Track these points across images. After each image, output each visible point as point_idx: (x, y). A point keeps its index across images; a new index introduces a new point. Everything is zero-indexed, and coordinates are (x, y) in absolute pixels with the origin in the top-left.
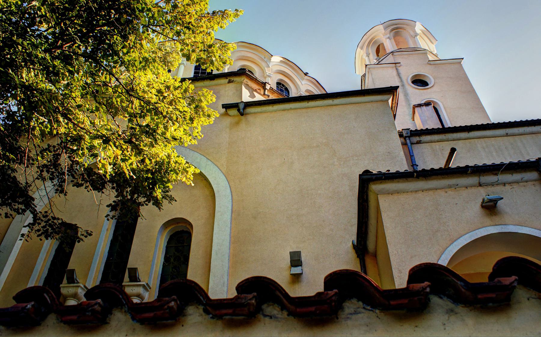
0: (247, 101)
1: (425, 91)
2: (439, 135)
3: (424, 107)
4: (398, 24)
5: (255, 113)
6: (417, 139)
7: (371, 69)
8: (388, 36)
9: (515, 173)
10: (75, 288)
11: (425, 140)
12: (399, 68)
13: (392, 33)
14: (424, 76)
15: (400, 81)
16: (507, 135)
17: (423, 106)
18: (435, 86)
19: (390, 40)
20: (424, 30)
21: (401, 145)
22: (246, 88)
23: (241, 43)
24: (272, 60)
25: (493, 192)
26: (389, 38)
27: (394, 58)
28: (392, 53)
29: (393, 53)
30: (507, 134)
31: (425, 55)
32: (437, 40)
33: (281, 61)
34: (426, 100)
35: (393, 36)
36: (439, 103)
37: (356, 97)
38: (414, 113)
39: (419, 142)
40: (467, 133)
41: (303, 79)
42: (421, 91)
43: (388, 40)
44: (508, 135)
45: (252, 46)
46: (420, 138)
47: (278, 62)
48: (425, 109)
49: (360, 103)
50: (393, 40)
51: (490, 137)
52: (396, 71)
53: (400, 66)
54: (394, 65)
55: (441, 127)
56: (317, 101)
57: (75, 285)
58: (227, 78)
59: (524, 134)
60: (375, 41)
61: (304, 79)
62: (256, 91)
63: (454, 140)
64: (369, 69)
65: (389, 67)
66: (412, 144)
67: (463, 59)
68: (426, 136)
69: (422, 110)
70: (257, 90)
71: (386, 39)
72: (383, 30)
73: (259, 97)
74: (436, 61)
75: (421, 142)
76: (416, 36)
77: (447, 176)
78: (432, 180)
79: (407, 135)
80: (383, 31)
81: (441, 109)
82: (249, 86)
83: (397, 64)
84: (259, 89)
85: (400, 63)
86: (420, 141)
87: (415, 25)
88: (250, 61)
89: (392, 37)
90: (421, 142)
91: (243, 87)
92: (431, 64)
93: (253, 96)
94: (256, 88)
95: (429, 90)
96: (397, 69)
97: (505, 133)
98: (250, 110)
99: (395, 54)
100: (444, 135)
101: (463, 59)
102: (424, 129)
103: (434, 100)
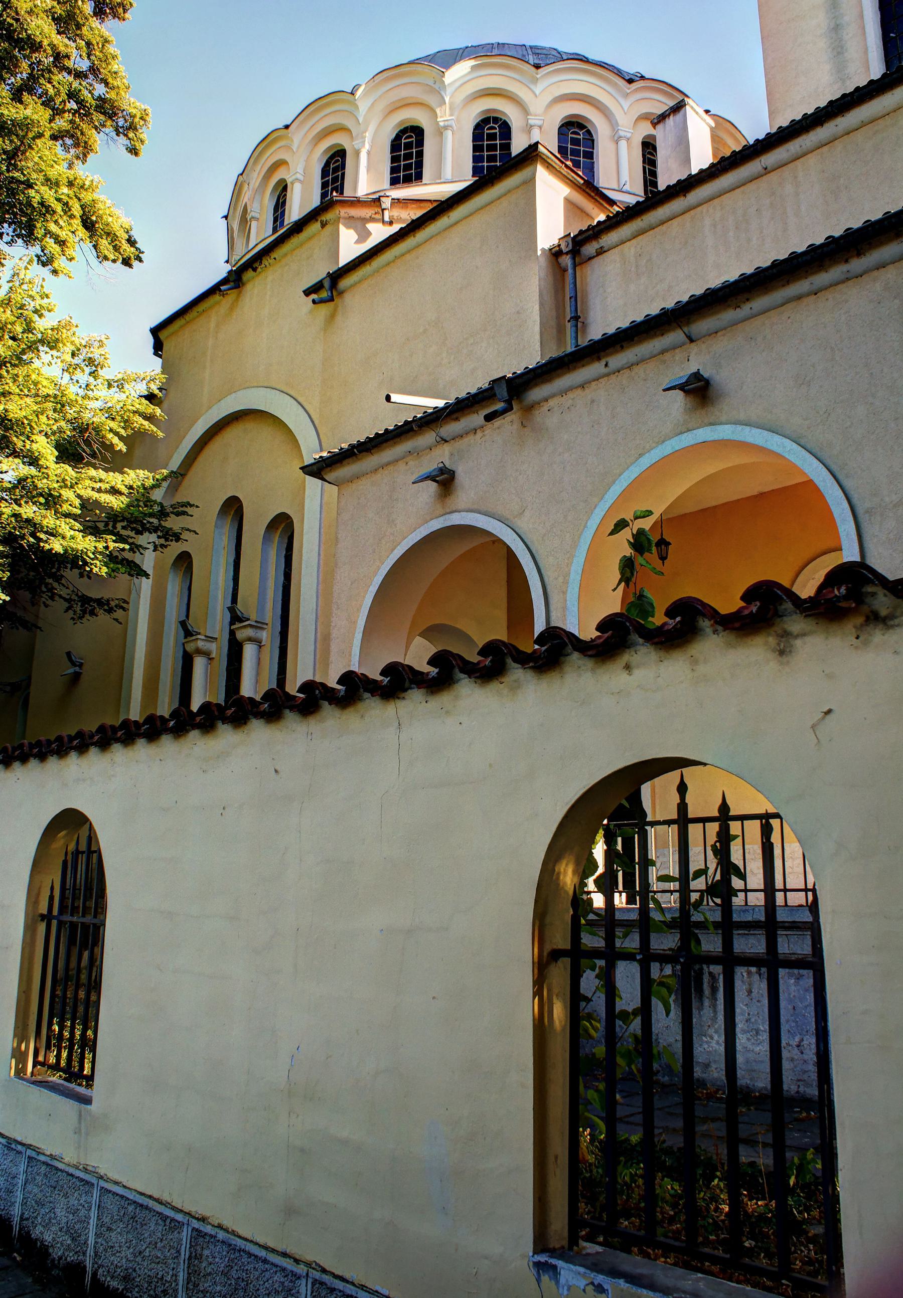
0: (358, 255)
5: (352, 286)
9: (482, 409)
10: (194, 642)
11: (609, 242)
16: (767, 171)
17: (669, 115)
22: (348, 227)
23: (381, 74)
24: (446, 83)
25: (442, 456)
30: (766, 169)
33: (474, 68)
39: (601, 252)
40: (682, 198)
41: (535, 81)
44: (769, 168)
45: (402, 69)
46: (598, 242)
47: (469, 73)
49: (492, 202)
56: (426, 226)
57: (194, 638)
58: (317, 220)
59: (804, 155)
61: (537, 79)
62: (372, 220)
63: (663, 223)
68: (609, 235)
70: (373, 216)
73: (379, 233)
77: (399, 440)
78: (383, 450)
82: (355, 216)
84: (376, 213)
88: (410, 104)
91: (341, 227)
93: (364, 235)
94: (370, 214)
97: (760, 168)
98: (344, 283)
100: (639, 219)
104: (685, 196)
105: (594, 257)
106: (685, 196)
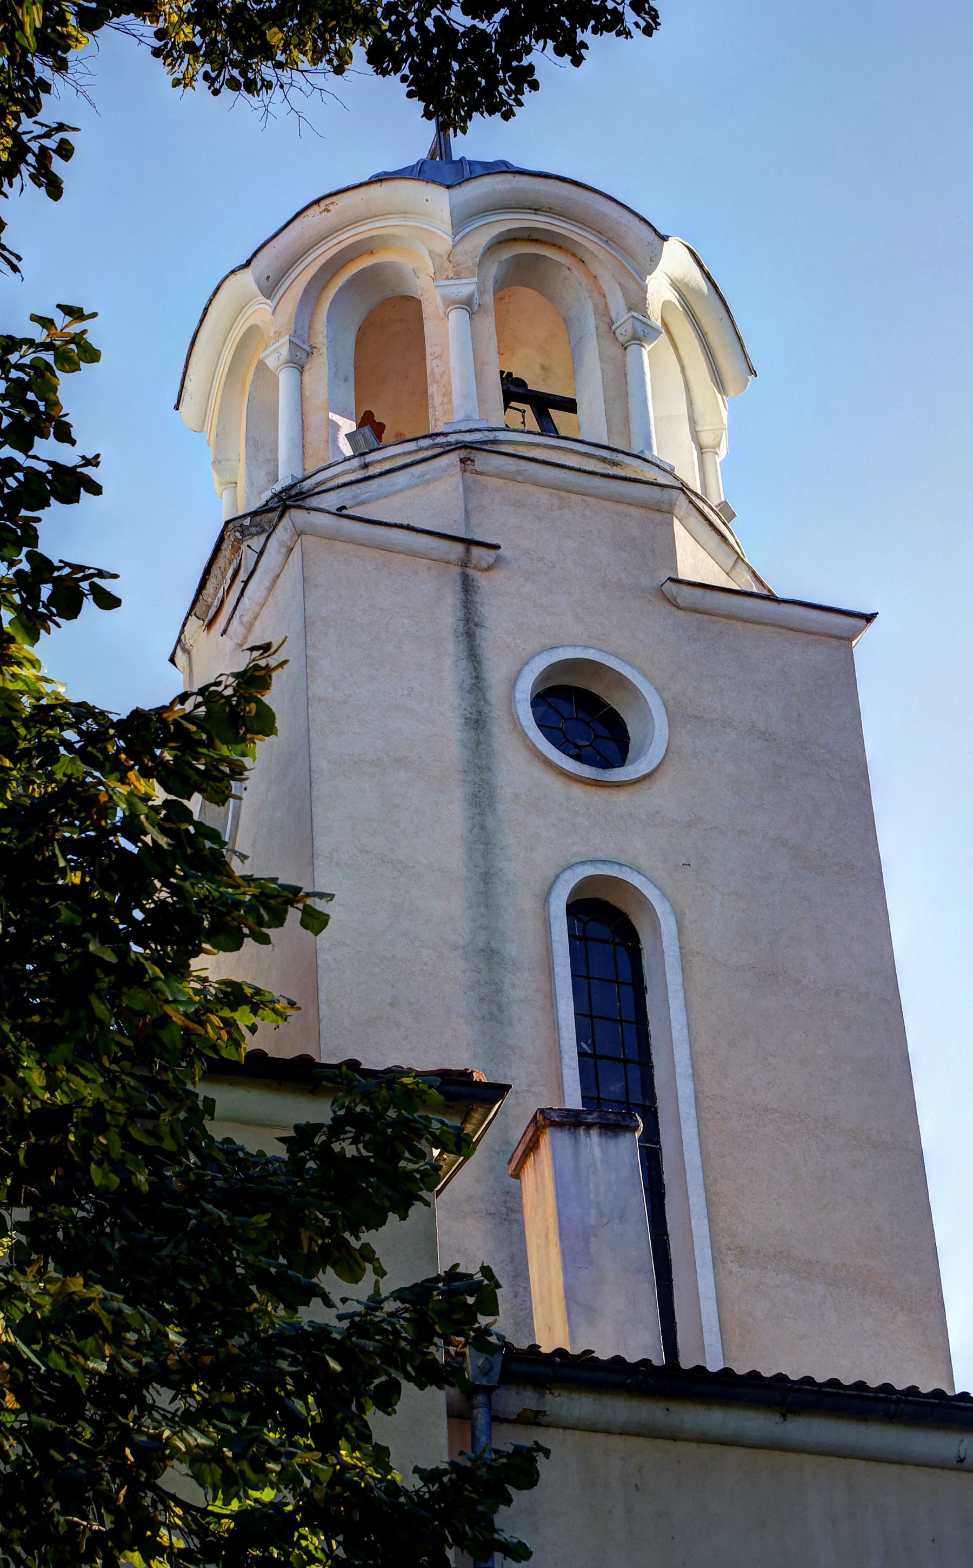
1: (598, 796)
2: (635, 1403)
3: (594, 1133)
4: (550, 211)
6: (527, 1399)
7: (308, 540)
8: (466, 287)
12: (482, 580)
13: (493, 270)
14: (620, 681)
15: (469, 681)
18: (662, 785)
19: (472, 315)
20: (697, 292)
21: (445, 1416)
26: (467, 304)
27: (467, 490)
28: (463, 453)
29: (474, 455)
30: (961, 1460)
31: (658, 516)
32: (753, 372)
34: (590, 871)
35: (496, 282)
36: (661, 908)
37: (269, 1088)
38: (532, 1146)
42: (577, 790)
43: (457, 317)
46: (542, 1396)
48: (597, 1151)
50: (488, 324)
51: (878, 1460)
52: (460, 595)
53: (489, 568)
54: (459, 548)
55: (659, 1360)
60: (374, 268)
63: (704, 1439)
64: (300, 534)
65: (422, 556)
66: (496, 1419)
67: (869, 618)
68: (576, 1396)
69: (576, 1155)
71: (451, 303)
72: (449, 228)
74: (708, 593)
75: (542, 1419)
76: (638, 339)
79: (484, 1381)
80: (444, 238)
81: (660, 953)
83: (476, 551)
85: (496, 547)
86: (538, 1413)
87: (654, 260)
89: (489, 299)
90: (542, 1419)
92: (680, 601)
95: (622, 797)
96: (467, 586)
99: (483, 461)
100: (662, 1405)
101: (869, 618)
102: (575, 1350)
103: (635, 880)
104: (784, 1416)
105: (506, 1421)
106: (784, 1416)
